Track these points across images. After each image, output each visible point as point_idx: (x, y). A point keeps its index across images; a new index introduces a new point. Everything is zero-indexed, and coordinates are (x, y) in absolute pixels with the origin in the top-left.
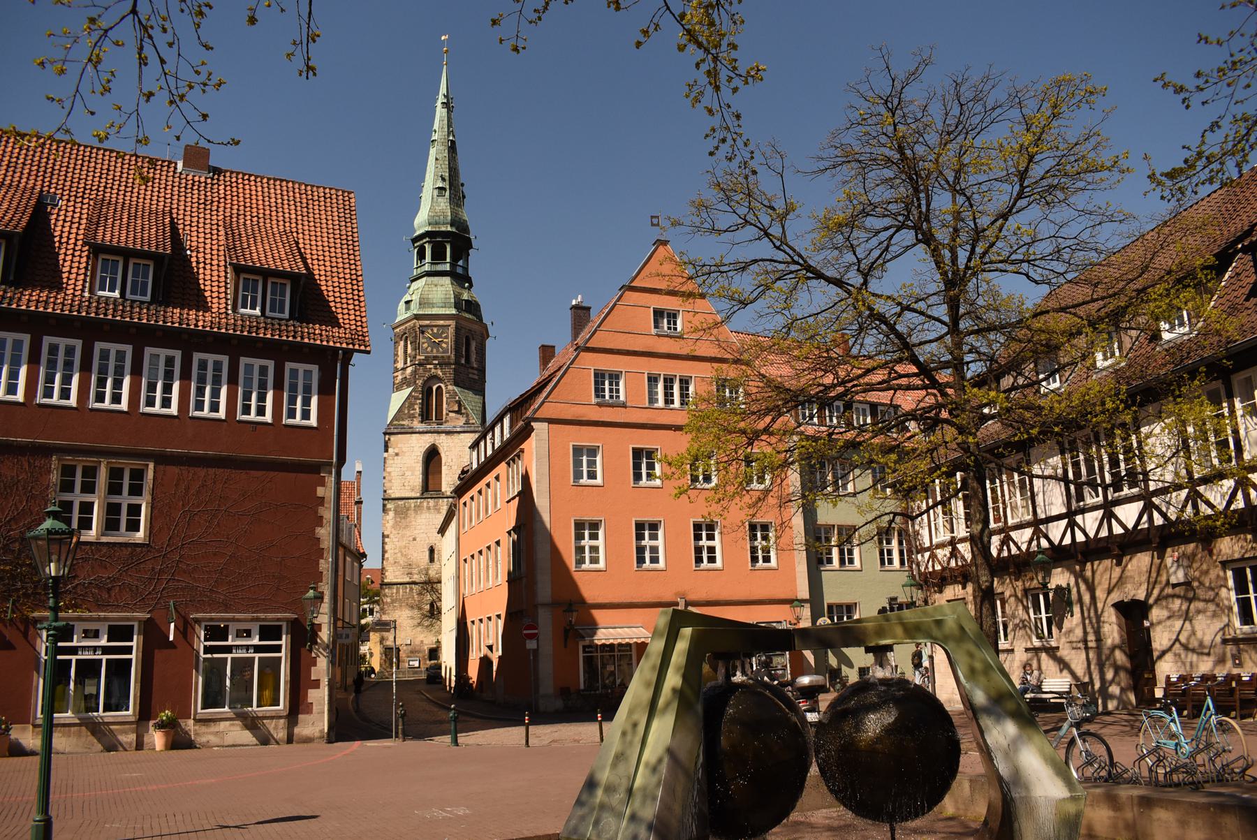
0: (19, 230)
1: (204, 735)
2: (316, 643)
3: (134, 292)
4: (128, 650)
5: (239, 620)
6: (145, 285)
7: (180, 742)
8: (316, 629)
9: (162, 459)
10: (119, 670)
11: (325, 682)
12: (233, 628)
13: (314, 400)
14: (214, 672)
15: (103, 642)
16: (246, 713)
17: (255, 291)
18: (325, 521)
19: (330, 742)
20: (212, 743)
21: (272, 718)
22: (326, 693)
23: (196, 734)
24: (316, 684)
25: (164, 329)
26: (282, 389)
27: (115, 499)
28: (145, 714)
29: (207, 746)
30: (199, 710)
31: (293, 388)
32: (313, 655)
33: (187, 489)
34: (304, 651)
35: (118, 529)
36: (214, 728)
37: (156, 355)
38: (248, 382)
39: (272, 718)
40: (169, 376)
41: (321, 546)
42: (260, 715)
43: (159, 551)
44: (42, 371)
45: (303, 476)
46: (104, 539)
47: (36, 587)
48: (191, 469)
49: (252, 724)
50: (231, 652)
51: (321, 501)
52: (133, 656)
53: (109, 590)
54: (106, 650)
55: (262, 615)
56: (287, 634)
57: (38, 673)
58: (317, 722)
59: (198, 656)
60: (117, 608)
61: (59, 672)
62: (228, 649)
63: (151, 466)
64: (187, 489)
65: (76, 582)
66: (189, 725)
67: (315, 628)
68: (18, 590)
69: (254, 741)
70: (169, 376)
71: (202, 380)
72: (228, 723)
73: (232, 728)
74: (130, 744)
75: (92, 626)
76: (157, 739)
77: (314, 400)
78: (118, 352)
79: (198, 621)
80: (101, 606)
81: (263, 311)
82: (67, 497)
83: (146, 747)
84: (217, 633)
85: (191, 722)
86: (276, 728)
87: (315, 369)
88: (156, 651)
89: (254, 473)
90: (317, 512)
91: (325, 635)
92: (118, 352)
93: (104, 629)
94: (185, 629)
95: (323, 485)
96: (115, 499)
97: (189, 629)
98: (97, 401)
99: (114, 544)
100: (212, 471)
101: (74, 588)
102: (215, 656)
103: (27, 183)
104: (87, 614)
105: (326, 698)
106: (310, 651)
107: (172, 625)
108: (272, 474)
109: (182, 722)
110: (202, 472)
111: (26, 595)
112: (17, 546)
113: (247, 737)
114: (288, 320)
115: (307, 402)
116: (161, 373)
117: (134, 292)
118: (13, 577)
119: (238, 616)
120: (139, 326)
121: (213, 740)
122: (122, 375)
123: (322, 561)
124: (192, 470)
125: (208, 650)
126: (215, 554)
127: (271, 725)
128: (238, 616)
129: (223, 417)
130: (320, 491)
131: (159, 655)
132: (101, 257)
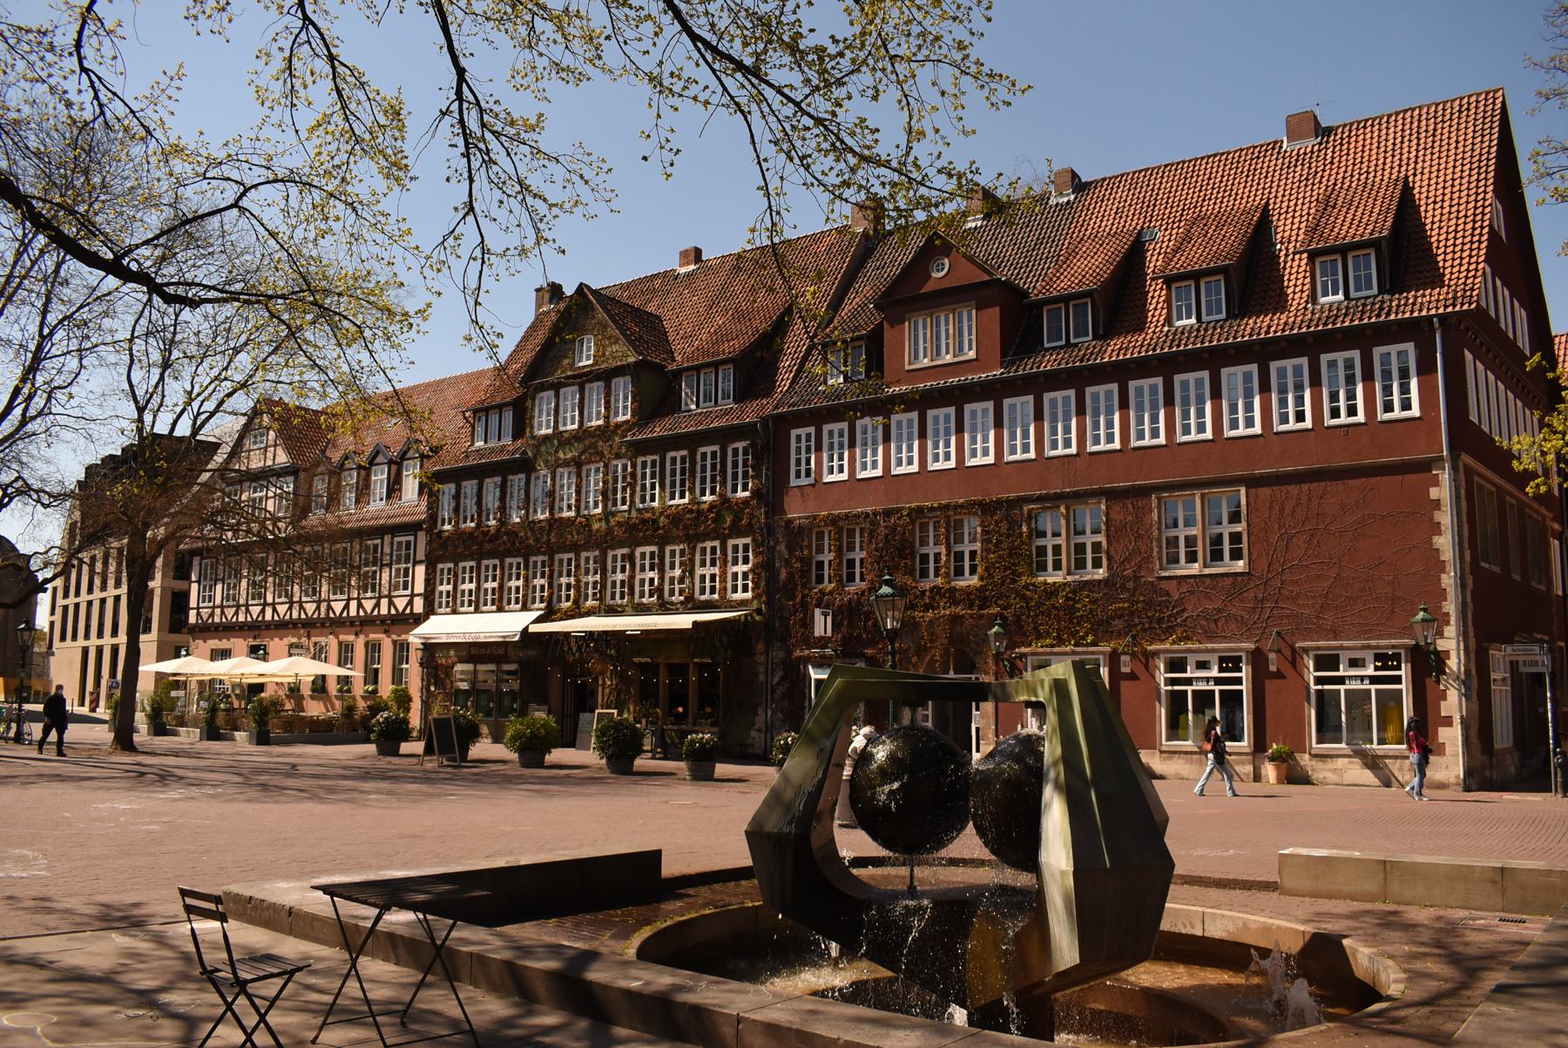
0: (1385, 233)
1: (1319, 771)
2: (1445, 673)
3: (1358, 289)
4: (1238, 681)
5: (1348, 648)
6: (1368, 277)
7: (1292, 776)
8: (1441, 658)
9: (1252, 482)
10: (1232, 701)
11: (1457, 720)
12: (1344, 657)
13: (1414, 384)
14: (1325, 704)
15: (1214, 673)
16: (1365, 750)
17: (1335, 273)
18: (1443, 528)
19: (1467, 789)
20: (1328, 781)
21: (1396, 757)
22: (1460, 732)
23: (1313, 770)
24: (1448, 722)
25: (1236, 346)
26: (1173, 405)
27: (1080, 539)
28: (1260, 746)
29: (1323, 783)
30: (1314, 745)
31: (1387, 375)
32: (1442, 687)
33: (1282, 510)
34: (1430, 682)
35: (1222, 560)
36: (1331, 764)
37: (1232, 375)
38: (1387, 375)
39: (1396, 757)
40: (1350, 380)
41: (1442, 558)
42: (1379, 753)
43: (1259, 578)
44: (1274, 397)
45: (1411, 478)
46: (1207, 571)
47: (1151, 622)
48: (1283, 488)
49: (1373, 763)
50: (1344, 683)
51: (1437, 504)
52: (1243, 687)
53: (1216, 621)
54: (1218, 681)
55: (1373, 642)
56: (1406, 662)
57: (1309, 703)
58: (1450, 765)
59: (1308, 688)
60: (1226, 639)
61: (1177, 702)
62: (1189, 681)
63: (1243, 490)
64: (1282, 510)
65: (1186, 615)
66: (1304, 760)
67: (1442, 655)
68: (1136, 625)
69: (1376, 782)
70: (1350, 380)
71: (1283, 391)
72: (1346, 760)
73: (1351, 766)
74: (1248, 775)
75: (1202, 657)
76: (1270, 771)
77: (1414, 384)
78: (1399, 353)
79: (1306, 650)
80: (1211, 638)
81: (1199, 319)
82: (1172, 533)
83: (1263, 780)
84: (1327, 661)
85: (1307, 756)
86: (1401, 769)
87: (1410, 347)
88: (1267, 681)
89: (1352, 482)
90: (1432, 518)
91: (1453, 663)
92: (1399, 353)
93: (1214, 660)
94: (1294, 659)
95: (1436, 484)
96: (1080, 539)
97: (1298, 659)
98: (1333, 417)
99: (1216, 575)
100: (1305, 487)
101: (1185, 621)
102: (1326, 687)
103: (1399, 172)
104: (1197, 646)
105: (1460, 738)
106: (1438, 682)
107: (649, 660)
108: (1373, 480)
109: (1298, 756)
110: (1294, 489)
111: (1144, 630)
112: (1131, 585)
113: (1368, 776)
114: (1376, 296)
115: (1405, 389)
116: (1241, 391)
117: (1358, 289)
118: (1132, 614)
119: (1346, 643)
120: (1210, 350)
121: (1331, 777)
122: (1355, 384)
123: (1443, 576)
124: (1284, 488)
125: (1319, 681)
126: (1318, 577)
127: (1394, 766)
128: (1346, 643)
129: (1363, 420)
130: (1434, 493)
131: (1270, 686)
132: (1174, 286)
